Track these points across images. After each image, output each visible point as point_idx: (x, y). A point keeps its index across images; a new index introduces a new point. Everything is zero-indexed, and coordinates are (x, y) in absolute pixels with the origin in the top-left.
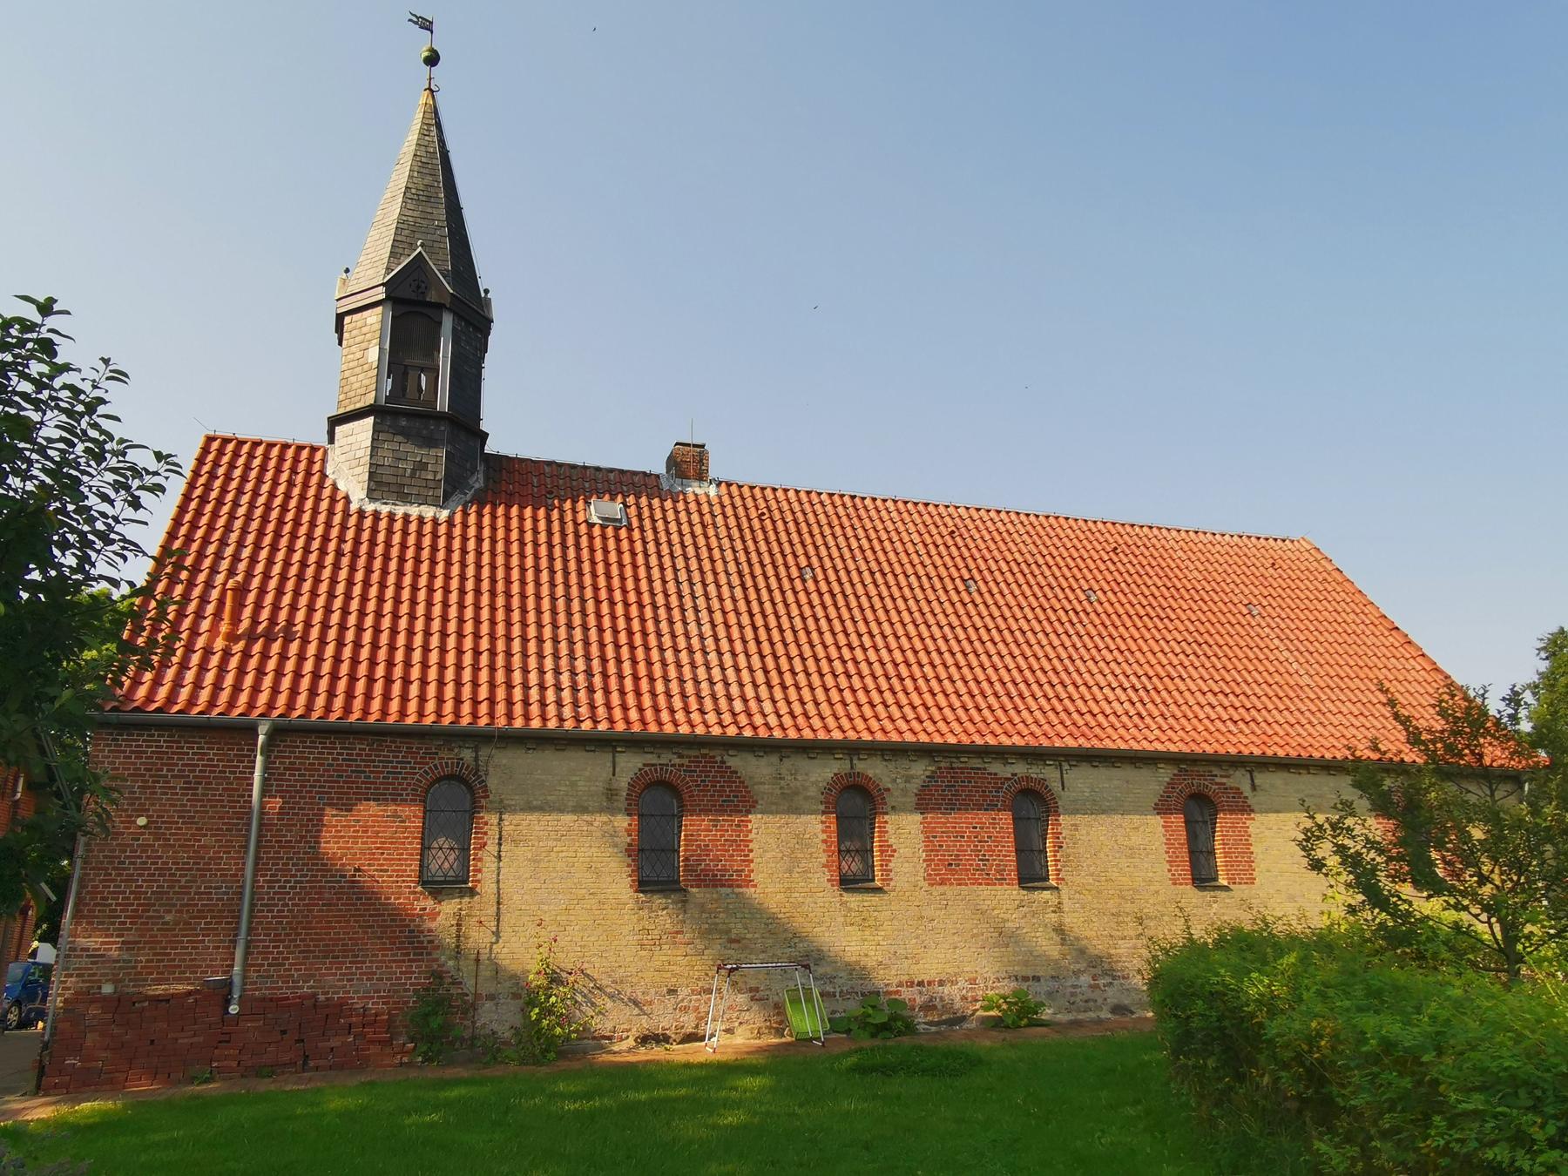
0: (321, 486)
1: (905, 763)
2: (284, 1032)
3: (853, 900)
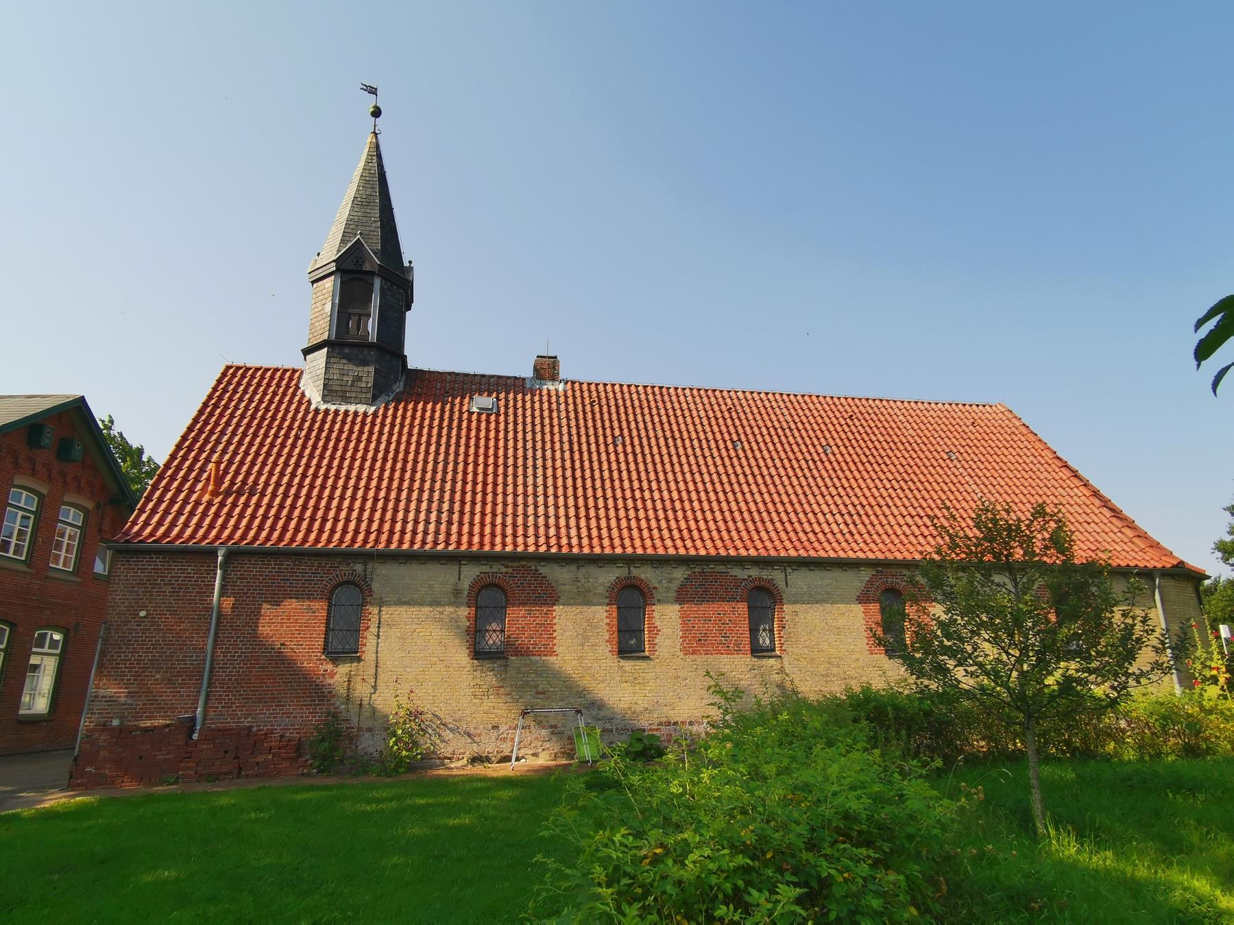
0: (294, 394)
1: (668, 569)
2: (226, 752)
3: (628, 665)
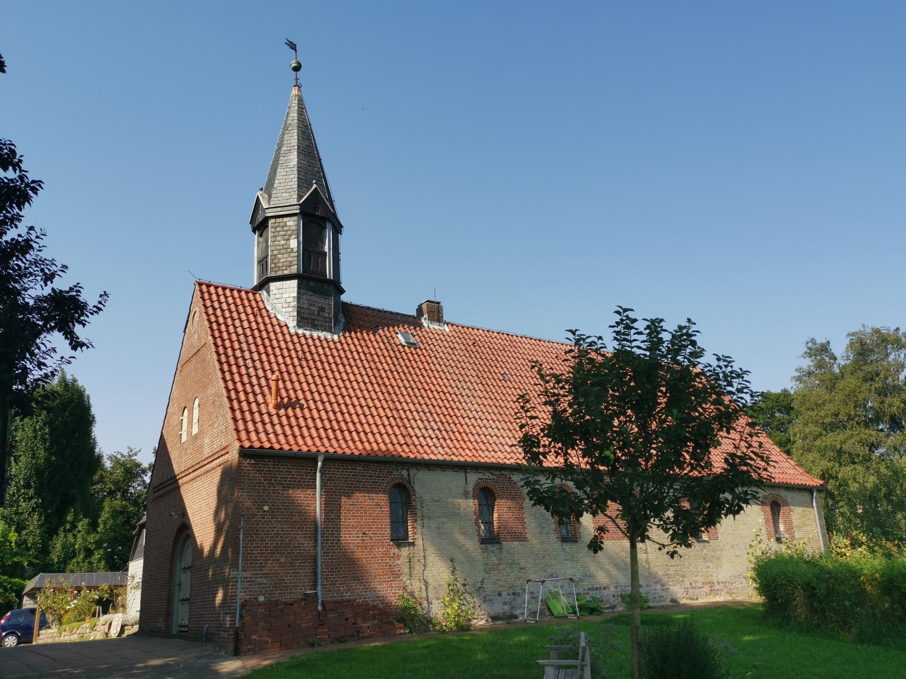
3: (567, 547)
